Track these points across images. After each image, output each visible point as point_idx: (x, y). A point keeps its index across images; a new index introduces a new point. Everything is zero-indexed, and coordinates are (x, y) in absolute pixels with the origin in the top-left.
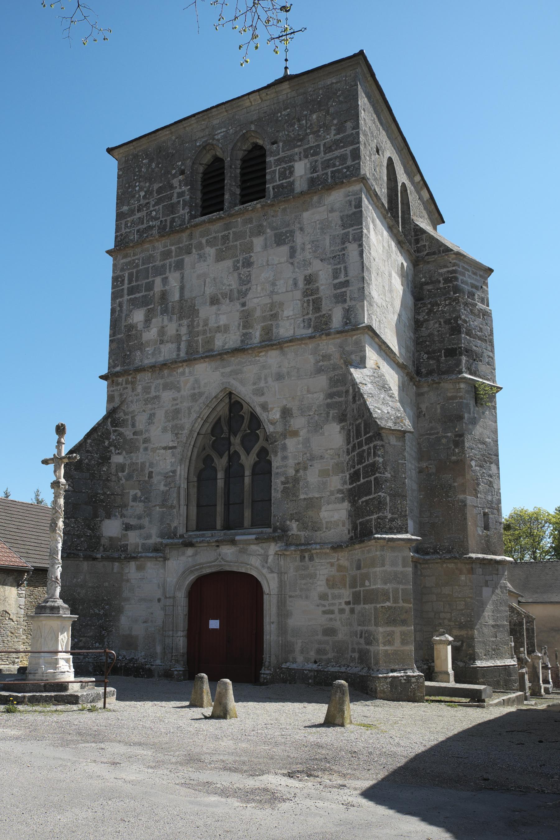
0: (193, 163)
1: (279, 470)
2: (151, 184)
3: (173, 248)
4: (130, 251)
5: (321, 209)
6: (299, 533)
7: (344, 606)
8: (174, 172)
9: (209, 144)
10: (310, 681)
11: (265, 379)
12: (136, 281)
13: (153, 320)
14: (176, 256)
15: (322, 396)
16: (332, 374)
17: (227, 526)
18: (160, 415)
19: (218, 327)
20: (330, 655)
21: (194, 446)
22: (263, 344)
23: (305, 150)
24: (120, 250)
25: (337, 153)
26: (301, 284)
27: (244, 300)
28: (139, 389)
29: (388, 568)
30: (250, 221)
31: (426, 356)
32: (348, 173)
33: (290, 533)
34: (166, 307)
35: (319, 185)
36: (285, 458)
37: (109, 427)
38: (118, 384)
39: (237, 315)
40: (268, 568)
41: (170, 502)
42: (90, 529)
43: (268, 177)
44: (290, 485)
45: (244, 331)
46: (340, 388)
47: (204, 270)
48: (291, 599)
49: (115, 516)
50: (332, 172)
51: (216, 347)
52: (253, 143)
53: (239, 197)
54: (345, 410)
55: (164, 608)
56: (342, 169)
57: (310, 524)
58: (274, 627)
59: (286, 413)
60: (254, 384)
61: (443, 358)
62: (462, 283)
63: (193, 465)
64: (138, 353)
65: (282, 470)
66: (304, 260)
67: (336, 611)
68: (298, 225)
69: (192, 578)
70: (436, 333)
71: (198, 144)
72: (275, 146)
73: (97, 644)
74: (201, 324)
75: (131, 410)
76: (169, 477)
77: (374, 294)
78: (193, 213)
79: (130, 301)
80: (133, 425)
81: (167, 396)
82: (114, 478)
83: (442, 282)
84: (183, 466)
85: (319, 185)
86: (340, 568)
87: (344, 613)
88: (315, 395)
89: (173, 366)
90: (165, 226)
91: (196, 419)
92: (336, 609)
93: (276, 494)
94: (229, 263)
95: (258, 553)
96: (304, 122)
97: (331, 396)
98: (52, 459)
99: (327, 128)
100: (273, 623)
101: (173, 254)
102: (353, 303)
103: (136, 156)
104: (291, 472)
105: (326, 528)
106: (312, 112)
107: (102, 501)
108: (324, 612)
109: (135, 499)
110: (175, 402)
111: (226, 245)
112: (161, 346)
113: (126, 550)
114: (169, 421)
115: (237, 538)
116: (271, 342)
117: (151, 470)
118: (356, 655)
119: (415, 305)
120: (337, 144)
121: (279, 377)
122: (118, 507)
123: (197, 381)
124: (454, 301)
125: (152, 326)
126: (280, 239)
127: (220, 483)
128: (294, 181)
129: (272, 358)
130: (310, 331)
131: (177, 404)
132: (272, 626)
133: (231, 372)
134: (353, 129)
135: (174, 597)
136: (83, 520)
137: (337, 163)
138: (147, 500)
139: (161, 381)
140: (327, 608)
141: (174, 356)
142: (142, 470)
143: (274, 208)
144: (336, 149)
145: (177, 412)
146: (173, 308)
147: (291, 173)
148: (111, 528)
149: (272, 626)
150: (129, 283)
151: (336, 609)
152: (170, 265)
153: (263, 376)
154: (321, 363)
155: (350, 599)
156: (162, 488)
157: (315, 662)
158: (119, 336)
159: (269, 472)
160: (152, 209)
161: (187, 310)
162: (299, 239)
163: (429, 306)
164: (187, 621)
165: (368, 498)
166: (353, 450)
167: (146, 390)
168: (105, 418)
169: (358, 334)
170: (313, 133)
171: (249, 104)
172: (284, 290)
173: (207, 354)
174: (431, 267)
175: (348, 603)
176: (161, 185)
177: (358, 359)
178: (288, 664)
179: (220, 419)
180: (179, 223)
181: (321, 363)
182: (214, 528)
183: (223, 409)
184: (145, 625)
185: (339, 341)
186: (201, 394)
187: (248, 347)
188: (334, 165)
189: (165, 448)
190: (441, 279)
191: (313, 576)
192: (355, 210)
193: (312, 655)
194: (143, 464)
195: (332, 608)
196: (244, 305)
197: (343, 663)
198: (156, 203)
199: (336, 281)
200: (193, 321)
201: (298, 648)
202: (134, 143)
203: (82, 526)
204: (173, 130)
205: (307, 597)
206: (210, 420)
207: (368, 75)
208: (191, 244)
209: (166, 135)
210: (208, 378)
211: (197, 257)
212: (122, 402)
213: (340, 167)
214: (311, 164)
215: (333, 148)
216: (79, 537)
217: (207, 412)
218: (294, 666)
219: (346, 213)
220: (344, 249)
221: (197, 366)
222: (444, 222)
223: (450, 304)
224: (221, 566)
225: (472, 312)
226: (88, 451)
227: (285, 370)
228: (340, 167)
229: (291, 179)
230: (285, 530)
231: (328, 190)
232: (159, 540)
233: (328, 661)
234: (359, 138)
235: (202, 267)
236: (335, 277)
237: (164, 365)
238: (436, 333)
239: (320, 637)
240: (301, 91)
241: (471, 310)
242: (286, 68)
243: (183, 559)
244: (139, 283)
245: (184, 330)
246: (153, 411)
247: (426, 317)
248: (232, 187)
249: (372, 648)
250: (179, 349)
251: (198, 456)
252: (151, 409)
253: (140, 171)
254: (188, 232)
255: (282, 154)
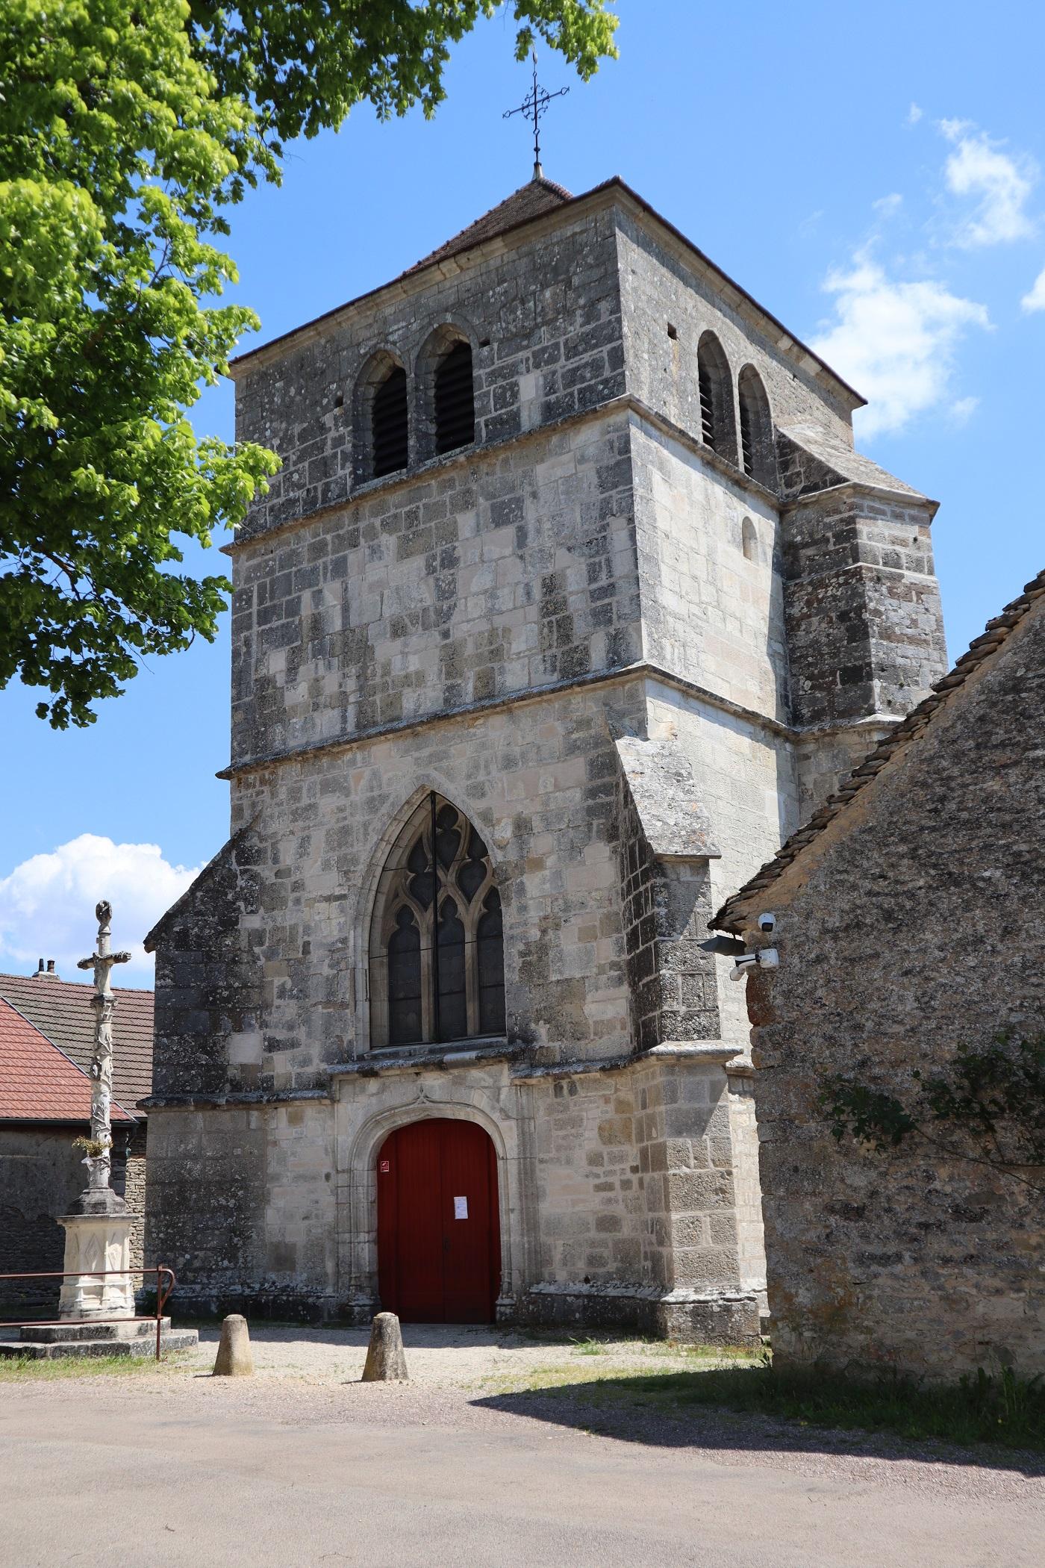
0: (356, 385)
1: (515, 932)
2: (289, 424)
3: (329, 537)
4: (261, 547)
5: (565, 458)
6: (551, 1044)
7: (629, 1175)
8: (325, 401)
9: (380, 350)
10: (577, 1315)
11: (486, 767)
12: (272, 598)
13: (301, 668)
14: (334, 552)
15: (577, 795)
16: (593, 754)
17: (439, 1036)
18: (318, 837)
19: (406, 677)
20: (612, 1266)
21: (377, 892)
22: (484, 703)
23: (534, 354)
24: (242, 544)
25: (586, 357)
26: (537, 593)
27: (445, 626)
28: (283, 794)
29: (682, 1104)
30: (450, 484)
31: (808, 684)
32: (606, 391)
33: (536, 1045)
34: (321, 644)
35: (561, 416)
36: (523, 909)
37: (234, 866)
38: (248, 786)
39: (436, 654)
40: (502, 1110)
41: (340, 996)
42: (207, 1053)
43: (477, 405)
44: (533, 958)
45: (449, 682)
46: (607, 779)
47: (380, 576)
48: (542, 1166)
49: (250, 1025)
50: (580, 391)
51: (405, 712)
52: (455, 341)
53: (434, 438)
54: (616, 819)
55: (335, 1192)
56: (596, 384)
57: (568, 1027)
58: (514, 1217)
59: (522, 827)
60: (469, 777)
61: (840, 686)
62: (869, 539)
63: (378, 927)
64: (279, 728)
65: (518, 931)
66: (541, 551)
67: (617, 1185)
68: (528, 489)
69: (379, 1133)
70: (824, 640)
71: (362, 351)
72: (486, 348)
73: (226, 1262)
74: (379, 672)
75: (270, 831)
76: (336, 950)
77: (667, 599)
78: (360, 472)
79: (261, 634)
80: (276, 860)
81: (328, 803)
82: (245, 957)
83: (832, 540)
84: (359, 930)
85: (560, 415)
86: (622, 1106)
87: (630, 1188)
88: (568, 793)
89: (335, 750)
90: (315, 497)
91: (377, 845)
92: (616, 1180)
93: (511, 976)
94: (418, 562)
95: (483, 1084)
96: (531, 304)
97: (592, 793)
98: (91, 960)
99: (568, 313)
100: (513, 1210)
101: (330, 548)
102: (623, 624)
103: (264, 376)
104: (535, 934)
105: (595, 1034)
106: (544, 286)
107: (227, 1000)
108: (599, 1188)
109: (282, 994)
110: (342, 815)
111: (414, 529)
112: (315, 714)
113: (269, 1089)
114: (333, 849)
115: (449, 1057)
116: (492, 701)
117: (306, 938)
118: (648, 1264)
119: (785, 588)
120: (588, 341)
121: (509, 763)
122: (255, 1009)
123: (375, 775)
124: (852, 577)
125: (299, 678)
126: (504, 514)
127: (426, 957)
128: (519, 409)
129: (495, 730)
130: (556, 677)
131: (345, 818)
132: (512, 1216)
133: (431, 755)
134: (612, 313)
135: (350, 1171)
136: (193, 1036)
137: (588, 375)
138: (302, 994)
139: (317, 778)
140: (602, 1180)
141: (337, 730)
142: (293, 940)
143: (488, 460)
144: (585, 351)
145: (345, 831)
146: (332, 644)
147: (515, 395)
148: (244, 1049)
149: (512, 1216)
150: (260, 603)
151: (616, 1180)
152: (325, 568)
153: (482, 763)
154: (574, 736)
155: (637, 1162)
156: (326, 971)
157: (587, 1280)
158: (247, 699)
159: (499, 935)
160: (292, 469)
161: (355, 649)
162: (531, 512)
163: (810, 589)
164: (375, 1212)
165: (648, 979)
166: (629, 894)
167: (295, 794)
168: (226, 850)
169: (632, 680)
170: (545, 323)
171: (441, 277)
172: (511, 606)
173: (389, 726)
174: (810, 513)
175: (635, 1170)
176: (305, 425)
177: (635, 724)
178: (541, 1286)
179: (420, 839)
180: (337, 492)
181: (574, 736)
182: (418, 1039)
183: (422, 821)
184: (307, 1222)
185: (602, 693)
186: (383, 798)
187: (456, 710)
188: (583, 379)
189: (329, 899)
190: (830, 534)
191: (576, 1122)
192: (619, 458)
193: (581, 1267)
194: (294, 927)
195: (610, 1179)
196: (446, 635)
197: (632, 1280)
198: (299, 457)
199: (594, 586)
200: (364, 668)
201: (557, 1255)
202: (259, 355)
203: (192, 1047)
204: (320, 329)
205: (569, 1162)
206: (403, 843)
207: (639, 211)
208: (357, 530)
209: (310, 338)
210: (392, 772)
211: (367, 551)
212: (256, 818)
213: (593, 382)
214: (545, 377)
215: (580, 348)
216: (187, 1068)
217: (395, 830)
218: (552, 1289)
219: (605, 463)
220: (604, 528)
221: (374, 748)
222: (864, 402)
223: (846, 583)
224: (425, 1110)
225: (891, 593)
226: (199, 913)
227: (517, 751)
228: (593, 382)
229: (514, 407)
230: (528, 1038)
231: (573, 424)
232: (324, 1066)
233: (608, 1278)
234: (621, 329)
235: (376, 571)
236: (592, 579)
237: (320, 750)
238: (824, 640)
239: (593, 1234)
240: (525, 249)
241: (890, 590)
242: (537, 165)
243: (362, 1099)
244: (276, 602)
245: (351, 685)
246: (306, 833)
247: (805, 610)
248: (421, 424)
249: (664, 1251)
250: (344, 719)
251: (387, 908)
252: (304, 829)
253: (271, 402)
254: (351, 508)
255: (498, 364)
